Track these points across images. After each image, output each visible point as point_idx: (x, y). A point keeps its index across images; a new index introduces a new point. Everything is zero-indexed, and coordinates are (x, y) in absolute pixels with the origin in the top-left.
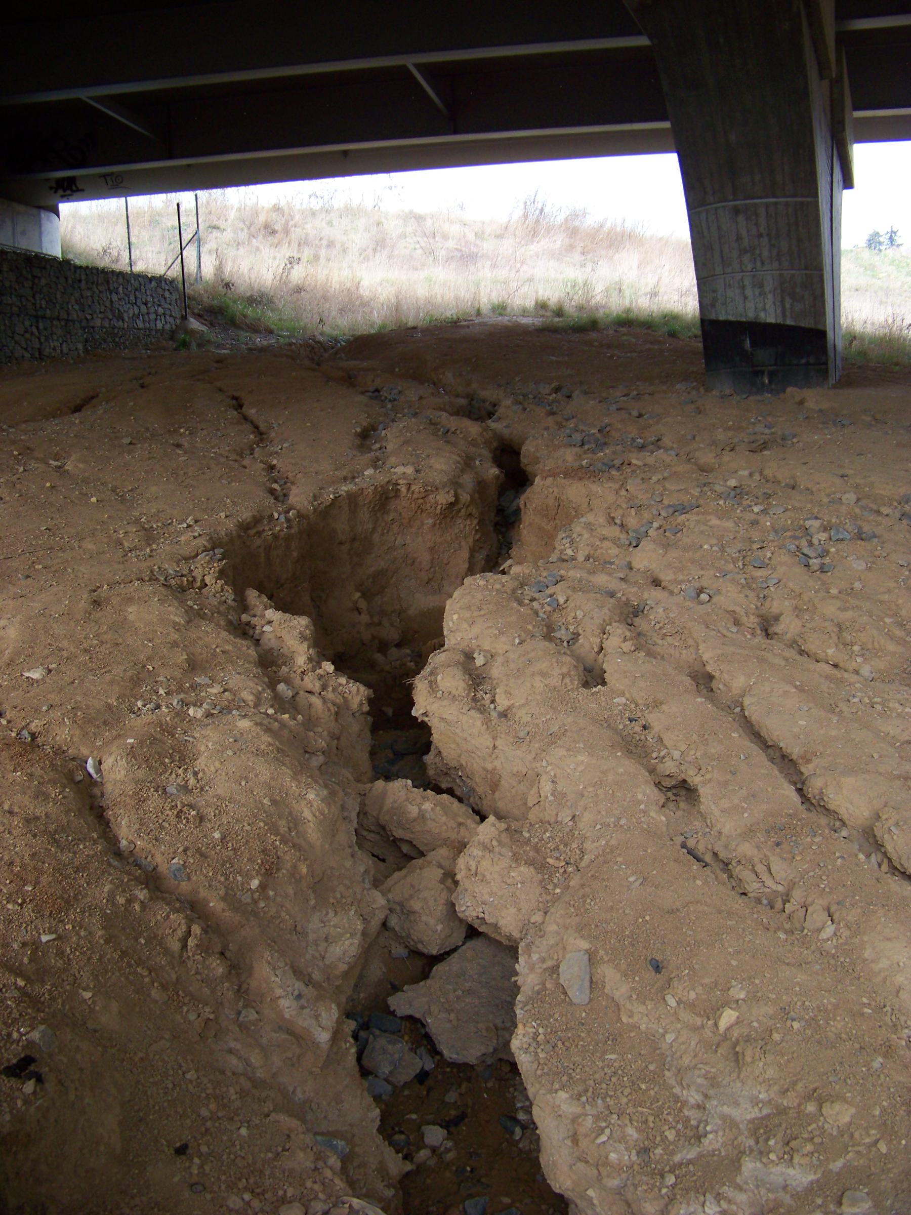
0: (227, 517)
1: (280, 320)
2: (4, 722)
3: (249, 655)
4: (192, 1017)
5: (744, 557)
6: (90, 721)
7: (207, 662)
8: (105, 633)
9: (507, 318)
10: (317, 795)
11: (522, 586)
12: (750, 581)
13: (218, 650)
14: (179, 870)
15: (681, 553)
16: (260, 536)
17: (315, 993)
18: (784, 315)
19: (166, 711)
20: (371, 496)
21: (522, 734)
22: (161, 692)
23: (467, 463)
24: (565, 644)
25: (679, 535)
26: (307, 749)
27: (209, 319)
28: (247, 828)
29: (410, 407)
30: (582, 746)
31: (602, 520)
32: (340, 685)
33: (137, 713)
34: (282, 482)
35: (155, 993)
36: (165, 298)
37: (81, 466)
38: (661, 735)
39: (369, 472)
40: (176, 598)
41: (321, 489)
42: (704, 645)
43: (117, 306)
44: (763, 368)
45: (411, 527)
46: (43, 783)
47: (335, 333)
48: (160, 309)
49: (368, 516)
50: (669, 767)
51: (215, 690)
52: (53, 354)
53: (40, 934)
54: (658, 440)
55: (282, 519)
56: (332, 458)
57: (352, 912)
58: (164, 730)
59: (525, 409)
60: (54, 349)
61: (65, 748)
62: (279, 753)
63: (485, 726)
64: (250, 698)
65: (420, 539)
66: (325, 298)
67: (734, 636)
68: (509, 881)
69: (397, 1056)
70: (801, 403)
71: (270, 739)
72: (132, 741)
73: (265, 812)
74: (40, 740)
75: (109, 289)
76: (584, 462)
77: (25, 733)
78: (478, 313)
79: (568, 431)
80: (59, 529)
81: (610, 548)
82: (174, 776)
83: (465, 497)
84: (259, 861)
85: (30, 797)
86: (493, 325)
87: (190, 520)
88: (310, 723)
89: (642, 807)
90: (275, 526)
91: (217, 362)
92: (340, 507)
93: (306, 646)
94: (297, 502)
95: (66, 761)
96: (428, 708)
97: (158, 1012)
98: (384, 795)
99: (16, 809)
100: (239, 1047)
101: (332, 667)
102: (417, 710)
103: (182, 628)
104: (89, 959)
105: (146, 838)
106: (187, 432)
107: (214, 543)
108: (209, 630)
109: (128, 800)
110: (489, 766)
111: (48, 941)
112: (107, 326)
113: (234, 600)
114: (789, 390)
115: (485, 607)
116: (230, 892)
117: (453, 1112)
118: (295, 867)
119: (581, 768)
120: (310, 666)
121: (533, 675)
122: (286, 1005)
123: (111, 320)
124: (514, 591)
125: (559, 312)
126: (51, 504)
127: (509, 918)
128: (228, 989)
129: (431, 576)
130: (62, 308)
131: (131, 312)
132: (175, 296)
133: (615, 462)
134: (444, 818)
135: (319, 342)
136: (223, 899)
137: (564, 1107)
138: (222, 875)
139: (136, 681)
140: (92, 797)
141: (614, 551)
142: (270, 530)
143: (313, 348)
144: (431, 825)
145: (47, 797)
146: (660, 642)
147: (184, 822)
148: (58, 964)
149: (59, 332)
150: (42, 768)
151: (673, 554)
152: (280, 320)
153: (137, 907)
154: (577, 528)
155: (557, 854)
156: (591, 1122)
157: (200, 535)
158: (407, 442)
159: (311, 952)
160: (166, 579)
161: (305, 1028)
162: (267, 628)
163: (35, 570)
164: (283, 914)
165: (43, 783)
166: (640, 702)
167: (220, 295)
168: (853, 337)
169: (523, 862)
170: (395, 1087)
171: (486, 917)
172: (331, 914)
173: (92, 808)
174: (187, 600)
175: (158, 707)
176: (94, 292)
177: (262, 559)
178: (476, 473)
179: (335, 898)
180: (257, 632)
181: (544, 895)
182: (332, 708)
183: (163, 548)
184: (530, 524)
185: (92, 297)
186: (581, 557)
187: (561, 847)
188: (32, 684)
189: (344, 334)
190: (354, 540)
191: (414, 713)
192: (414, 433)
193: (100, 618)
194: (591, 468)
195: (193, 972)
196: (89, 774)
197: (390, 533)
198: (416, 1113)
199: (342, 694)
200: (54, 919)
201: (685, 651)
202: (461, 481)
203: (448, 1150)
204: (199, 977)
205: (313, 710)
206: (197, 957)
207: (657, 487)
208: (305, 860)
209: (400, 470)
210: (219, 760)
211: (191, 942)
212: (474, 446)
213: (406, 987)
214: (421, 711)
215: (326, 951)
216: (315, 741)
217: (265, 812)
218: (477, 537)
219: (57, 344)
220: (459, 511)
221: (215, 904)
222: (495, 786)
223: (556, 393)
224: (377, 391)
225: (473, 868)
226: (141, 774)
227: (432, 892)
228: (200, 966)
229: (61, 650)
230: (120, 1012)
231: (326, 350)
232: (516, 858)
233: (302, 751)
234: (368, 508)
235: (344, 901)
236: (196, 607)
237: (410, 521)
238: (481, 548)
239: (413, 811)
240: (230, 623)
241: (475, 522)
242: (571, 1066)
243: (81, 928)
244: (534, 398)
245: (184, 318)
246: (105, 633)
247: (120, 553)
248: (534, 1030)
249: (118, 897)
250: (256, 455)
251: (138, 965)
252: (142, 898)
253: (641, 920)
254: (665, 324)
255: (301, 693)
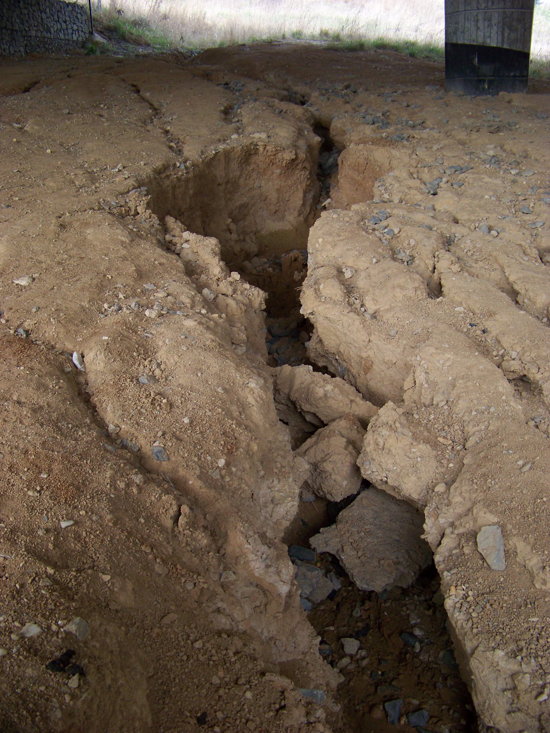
0: (145, 165)
1: (154, 37)
2: (3, 321)
3: (178, 266)
4: (190, 586)
5: (515, 206)
6: (70, 320)
7: (150, 271)
8: (72, 249)
9: (304, 41)
10: (257, 384)
11: (363, 219)
12: (523, 222)
13: (156, 263)
14: (161, 452)
15: (471, 201)
16: (168, 179)
17: (276, 553)
18: (503, 42)
19: (128, 312)
20: (239, 153)
21: (392, 333)
22: (121, 296)
23: (300, 133)
24: (405, 263)
25: (463, 187)
26: (233, 341)
27: (108, 35)
28: (209, 413)
29: (251, 95)
30: (447, 346)
31: (405, 175)
32: (245, 289)
33: (104, 313)
34: (176, 142)
35: (158, 568)
36: (78, 19)
37: (36, 127)
38: (500, 339)
39: (235, 136)
40: (121, 223)
41: (205, 147)
42: (509, 269)
43: (46, 22)
44: (485, 78)
45: (265, 175)
46: (42, 376)
47: (191, 47)
48: (75, 26)
49: (237, 167)
50: (515, 365)
51: (161, 294)
52: (4, 54)
53: (59, 521)
54: (423, 123)
55: (183, 167)
56: (207, 126)
57: (291, 480)
58: (128, 328)
59: (329, 99)
60: (4, 50)
61: (53, 343)
62: (220, 348)
63: (362, 325)
64: (187, 301)
65: (271, 183)
66: (183, 24)
67: (527, 263)
68: (410, 456)
69: (314, 580)
70: (509, 102)
71: (211, 336)
72: (107, 338)
73: (220, 399)
74: (33, 336)
75: (40, 10)
76: (384, 135)
77: (21, 331)
78: (284, 37)
79: (362, 114)
80: (26, 171)
81: (416, 195)
82: (142, 367)
83: (302, 155)
84: (222, 442)
85: (33, 389)
86: (295, 45)
87: (120, 166)
88: (230, 321)
89: (504, 398)
90: (178, 172)
91: (117, 62)
92: (219, 160)
93: (217, 260)
94: (190, 155)
95: (56, 355)
96: (315, 309)
97: (162, 585)
98: (292, 378)
99: (23, 400)
100: (225, 606)
101: (239, 276)
102: (304, 310)
103: (128, 246)
104: (102, 541)
105: (129, 422)
106: (106, 107)
107: (139, 183)
108: (148, 247)
109: (110, 389)
110: (364, 355)
111: (67, 527)
112: (40, 36)
113: (159, 224)
114: (501, 93)
115: (342, 234)
116: (203, 470)
117: (360, 624)
118: (248, 445)
119: (448, 364)
120: (223, 275)
121: (394, 287)
122: (256, 566)
123: (42, 32)
124: (358, 223)
125: (337, 38)
126: (19, 154)
127: (410, 484)
128: (213, 558)
129: (277, 209)
130: (8, 21)
131: (55, 27)
132: (85, 18)
133: (404, 135)
134: (340, 397)
135: (181, 53)
136: (200, 477)
137: (502, 664)
138: (195, 456)
139: (101, 288)
140: (78, 384)
141: (419, 197)
142: (175, 174)
143: (177, 56)
144: (331, 402)
145: (46, 388)
146: (474, 265)
147: (158, 408)
148: (77, 548)
149: (7, 38)
150: (39, 363)
151: (465, 201)
152: (154, 37)
153: (135, 490)
154: (389, 180)
155: (443, 434)
156: (528, 679)
157: (129, 177)
158: (257, 117)
159: (263, 514)
160: (109, 209)
161: (271, 584)
162: (185, 245)
163: (13, 201)
164: (243, 486)
165: (42, 376)
166: (477, 311)
167: (114, 19)
168: (537, 63)
169: (422, 441)
170: (313, 603)
171: (389, 481)
172: (276, 482)
173: (80, 394)
174: (128, 224)
175: (120, 308)
176: (29, 11)
177: (170, 195)
178: (306, 140)
179: (277, 468)
180: (178, 248)
181: (439, 468)
182: (243, 307)
183: (104, 186)
184: (345, 175)
185: (28, 14)
186: (396, 201)
187: (446, 428)
188: (21, 290)
189: (196, 48)
190: (227, 182)
191: (301, 312)
192: (260, 111)
193: (66, 238)
194: (389, 139)
195: (184, 545)
196: (75, 365)
197: (251, 179)
198: (333, 625)
199: (247, 296)
200: (70, 506)
201: (493, 273)
202: (298, 144)
203: (364, 658)
204: (189, 548)
205: (229, 309)
206: (186, 532)
207: (438, 153)
208: (256, 439)
209: (257, 135)
210: (177, 354)
211: (182, 520)
212: (300, 122)
213: (322, 530)
214: (309, 311)
215: (273, 511)
216: (238, 334)
217: (220, 399)
218: (308, 183)
219: (6, 47)
220: (298, 165)
221: (194, 483)
222: (367, 369)
223: (346, 89)
224: (227, 84)
225: (381, 444)
226: (117, 365)
227: (340, 457)
228: (189, 539)
229: (41, 262)
230: (133, 589)
231: (185, 58)
232: (415, 437)
233: (230, 343)
234: (237, 161)
235: (284, 470)
236: (135, 230)
237: (264, 171)
238: (310, 190)
239: (320, 392)
240: (159, 241)
241: (307, 173)
242: (501, 626)
243: (92, 513)
244: (333, 92)
245: (91, 33)
246: (72, 249)
247: (74, 189)
248: (464, 592)
249: (118, 482)
250: (155, 124)
251: (142, 544)
252: (138, 482)
253: (539, 501)
254: (408, 48)
255: (220, 295)
